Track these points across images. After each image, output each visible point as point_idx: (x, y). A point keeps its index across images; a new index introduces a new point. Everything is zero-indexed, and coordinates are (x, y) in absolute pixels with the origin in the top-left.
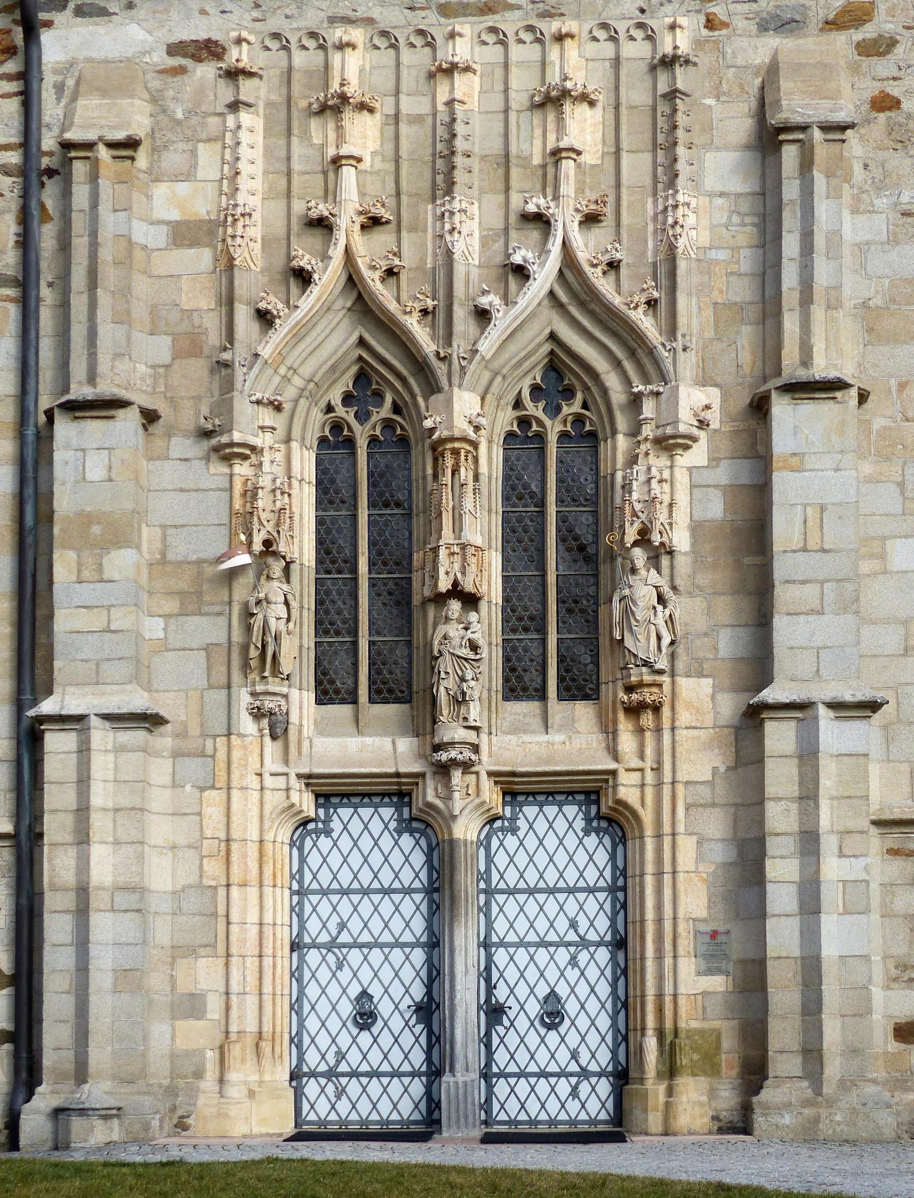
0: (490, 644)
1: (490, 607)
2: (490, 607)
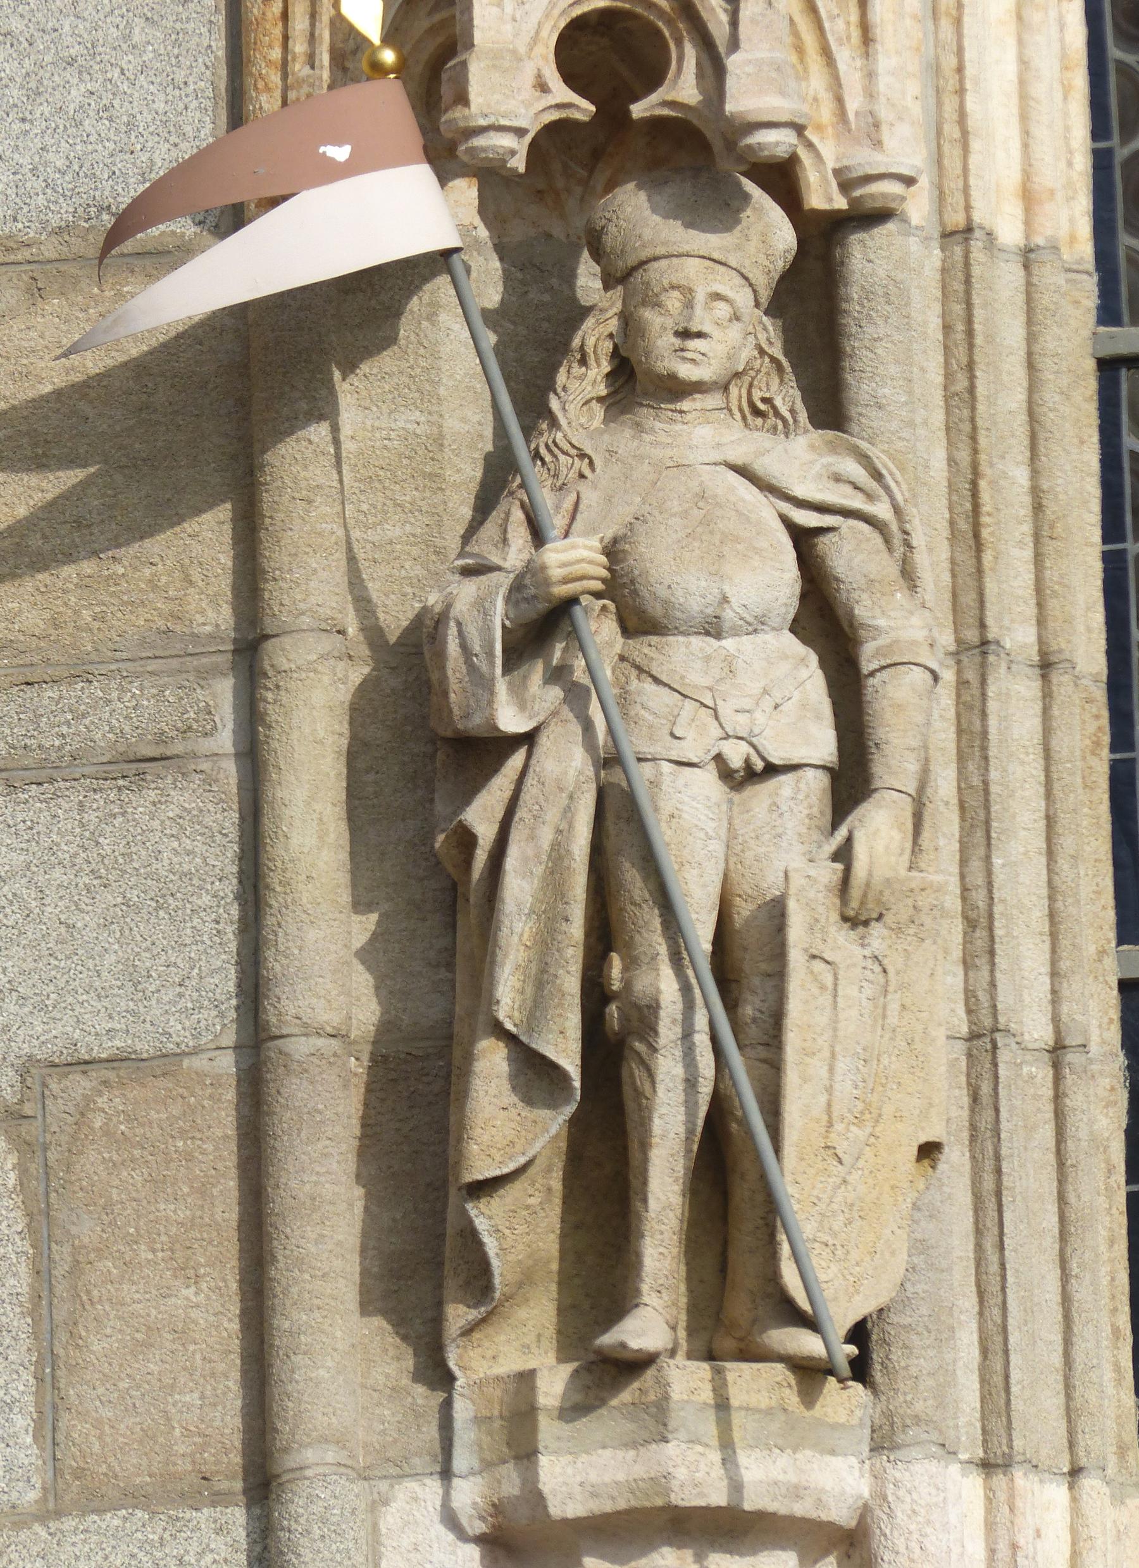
0: (977, 649)
1: (960, 290)
2: (960, 290)
